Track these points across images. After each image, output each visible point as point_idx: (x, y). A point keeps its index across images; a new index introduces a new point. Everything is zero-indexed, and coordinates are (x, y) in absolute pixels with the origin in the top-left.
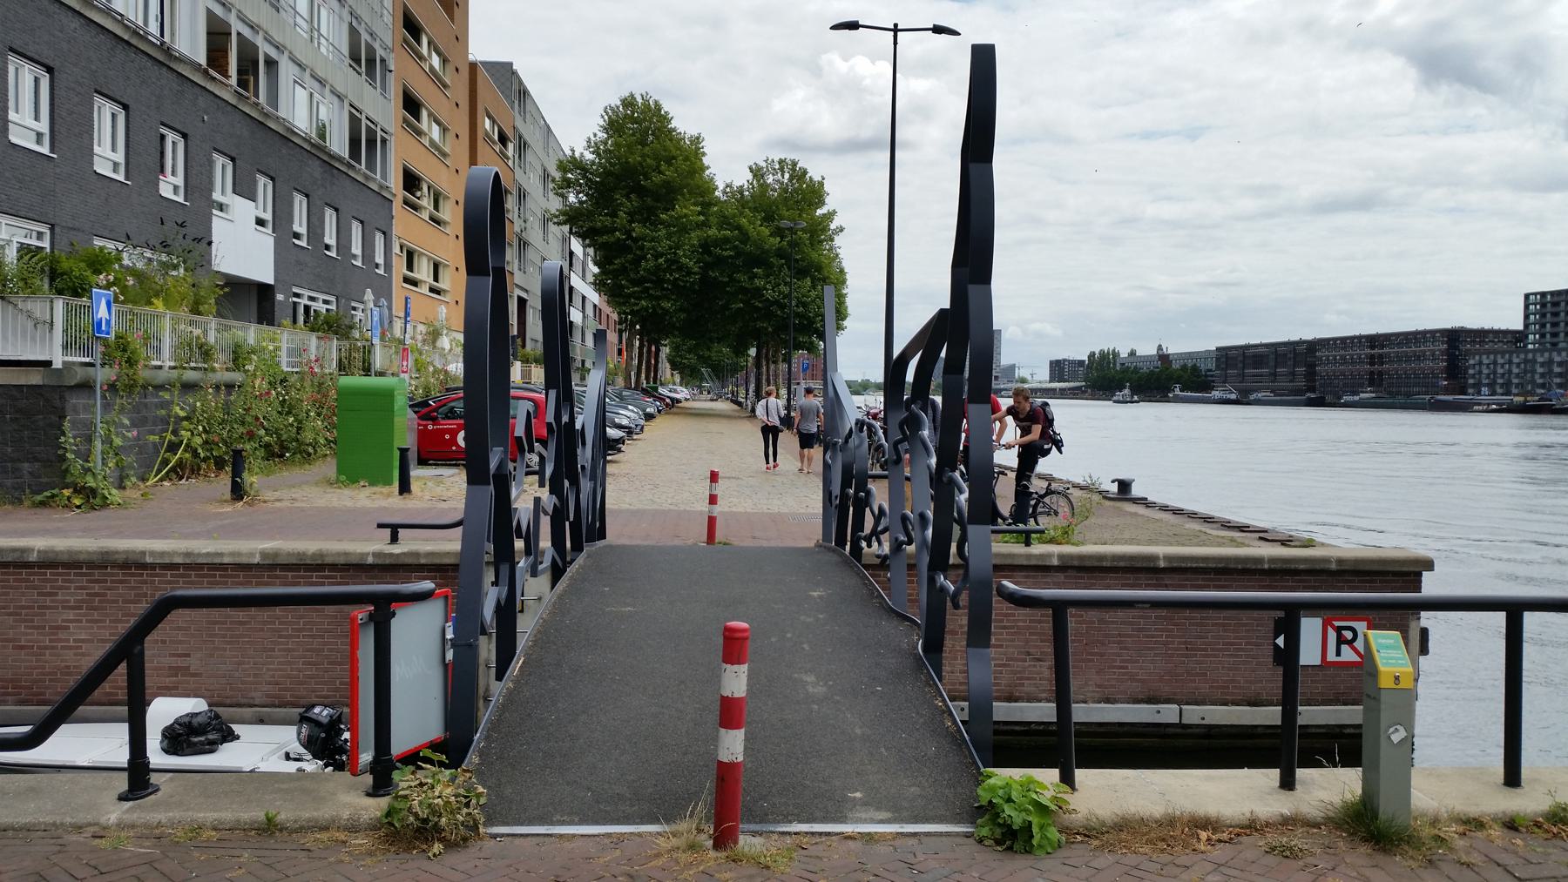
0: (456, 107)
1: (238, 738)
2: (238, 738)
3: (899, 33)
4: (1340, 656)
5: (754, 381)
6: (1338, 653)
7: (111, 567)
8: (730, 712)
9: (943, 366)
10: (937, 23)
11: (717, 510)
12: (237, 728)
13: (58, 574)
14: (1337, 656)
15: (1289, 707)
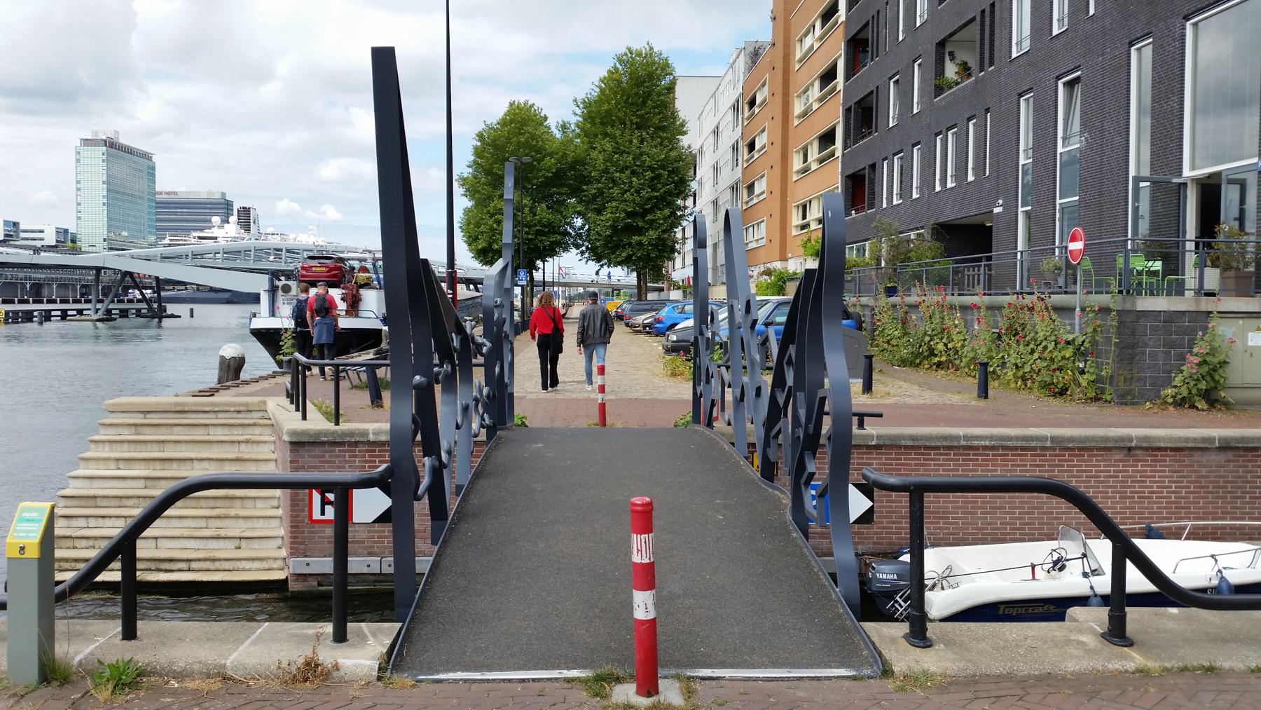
0: (1253, 355)
1: (976, 582)
2: (976, 582)
3: (1081, 560)
4: (324, 515)
5: (941, 401)
6: (323, 513)
7: (904, 447)
8: (647, 577)
9: (723, 250)
10: (1060, 623)
11: (608, 396)
12: (976, 579)
13: (881, 454)
14: (322, 515)
15: (341, 553)
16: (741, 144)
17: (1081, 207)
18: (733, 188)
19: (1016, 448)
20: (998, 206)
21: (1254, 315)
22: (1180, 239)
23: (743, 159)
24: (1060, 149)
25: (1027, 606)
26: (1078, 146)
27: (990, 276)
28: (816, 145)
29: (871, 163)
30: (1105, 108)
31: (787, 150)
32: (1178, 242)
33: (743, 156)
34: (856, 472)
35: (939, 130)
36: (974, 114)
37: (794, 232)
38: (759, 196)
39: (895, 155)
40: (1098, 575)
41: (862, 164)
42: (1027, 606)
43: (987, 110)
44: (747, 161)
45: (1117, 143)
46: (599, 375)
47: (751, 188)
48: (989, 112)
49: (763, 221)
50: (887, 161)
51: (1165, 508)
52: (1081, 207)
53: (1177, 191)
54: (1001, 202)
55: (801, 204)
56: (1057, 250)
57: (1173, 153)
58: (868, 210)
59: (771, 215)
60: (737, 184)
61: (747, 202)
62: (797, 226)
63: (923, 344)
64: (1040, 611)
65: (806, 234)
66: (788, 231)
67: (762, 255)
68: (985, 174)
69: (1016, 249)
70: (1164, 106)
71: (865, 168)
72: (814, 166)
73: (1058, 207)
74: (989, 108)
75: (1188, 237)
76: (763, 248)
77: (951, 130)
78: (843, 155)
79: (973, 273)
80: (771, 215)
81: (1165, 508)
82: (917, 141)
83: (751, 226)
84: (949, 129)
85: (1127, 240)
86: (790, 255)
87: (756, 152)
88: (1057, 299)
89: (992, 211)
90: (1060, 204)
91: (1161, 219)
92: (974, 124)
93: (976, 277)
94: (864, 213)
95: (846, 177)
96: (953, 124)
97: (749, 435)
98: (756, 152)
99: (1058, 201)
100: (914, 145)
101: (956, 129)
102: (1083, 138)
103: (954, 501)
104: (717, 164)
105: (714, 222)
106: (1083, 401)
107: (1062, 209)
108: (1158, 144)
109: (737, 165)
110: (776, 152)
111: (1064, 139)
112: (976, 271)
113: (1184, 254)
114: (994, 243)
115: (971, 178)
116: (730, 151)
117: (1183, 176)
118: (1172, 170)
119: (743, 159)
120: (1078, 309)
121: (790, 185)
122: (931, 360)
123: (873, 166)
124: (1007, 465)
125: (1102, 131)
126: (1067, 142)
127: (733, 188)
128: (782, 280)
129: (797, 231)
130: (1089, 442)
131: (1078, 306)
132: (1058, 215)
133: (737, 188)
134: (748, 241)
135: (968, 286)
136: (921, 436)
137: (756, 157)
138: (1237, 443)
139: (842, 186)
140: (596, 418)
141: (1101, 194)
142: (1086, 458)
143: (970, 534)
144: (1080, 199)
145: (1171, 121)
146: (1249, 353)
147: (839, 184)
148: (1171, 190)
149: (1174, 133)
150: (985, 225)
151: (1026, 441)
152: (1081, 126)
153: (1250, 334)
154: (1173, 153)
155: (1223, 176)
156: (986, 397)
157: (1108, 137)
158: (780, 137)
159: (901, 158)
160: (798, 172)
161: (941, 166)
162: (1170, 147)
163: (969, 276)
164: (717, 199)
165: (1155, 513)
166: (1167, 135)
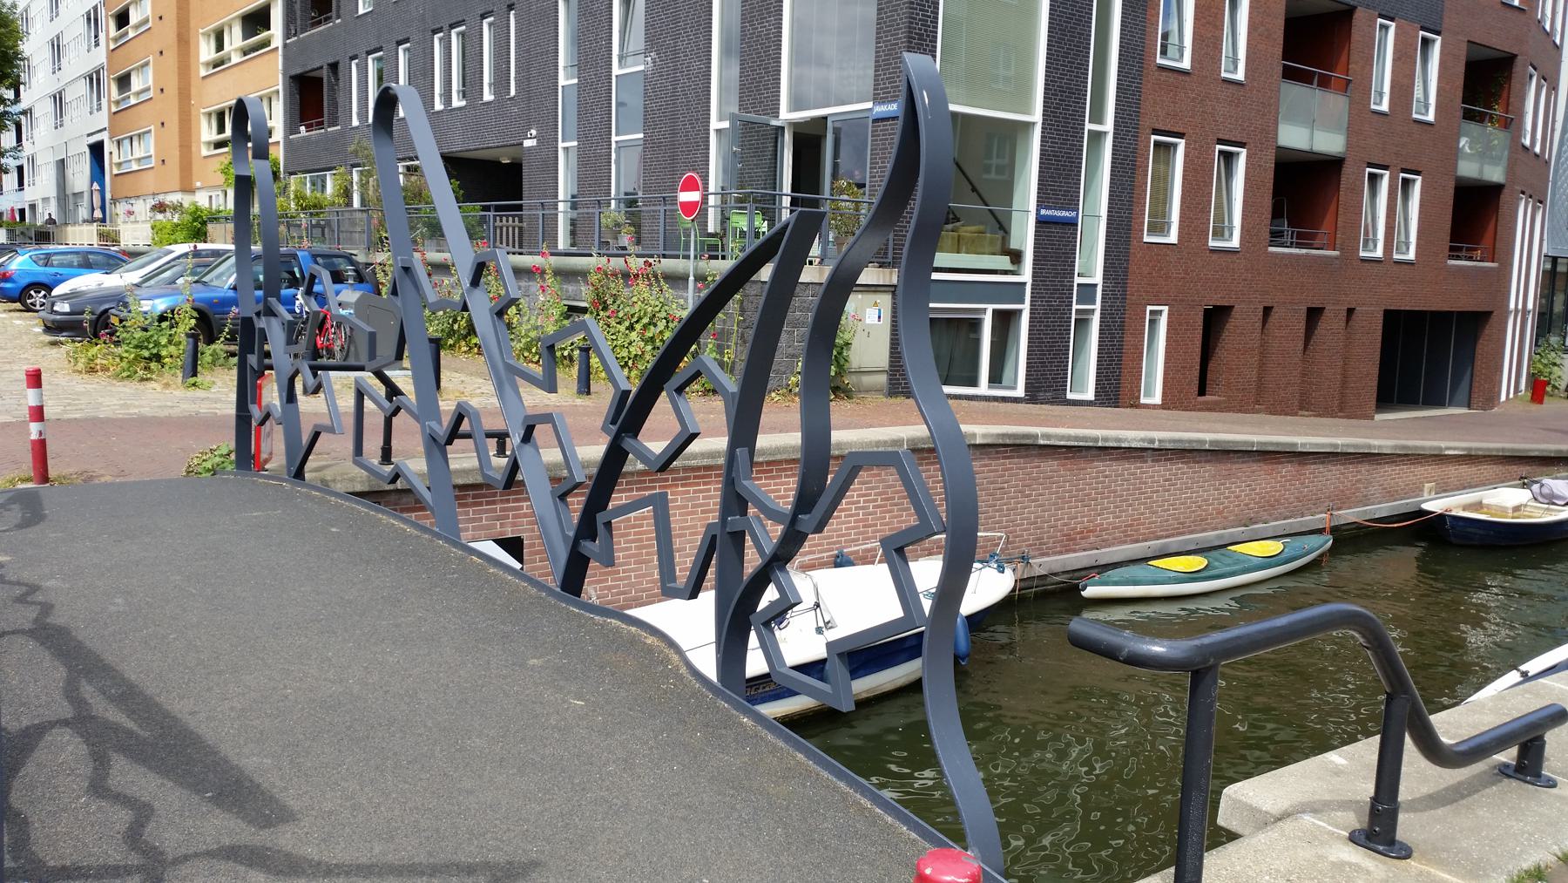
16: (102, 13)
17: (647, 148)
18: (91, 80)
19: (698, 468)
20: (531, 138)
21: (879, 289)
22: (777, 192)
23: (107, 35)
24: (616, 70)
25: (755, 685)
26: (641, 68)
27: (521, 229)
28: (237, 30)
29: (331, 60)
30: (679, 22)
31: (188, 31)
32: (775, 195)
33: (107, 32)
34: (498, 523)
35: (439, 26)
36: (490, 9)
37: (205, 152)
38: (138, 94)
39: (369, 53)
40: (831, 628)
41: (316, 61)
42: (755, 685)
43: (511, 7)
44: (116, 40)
45: (694, 70)
46: (28, 387)
47: (124, 82)
48: (512, 9)
49: (149, 131)
50: (357, 61)
51: (853, 528)
52: (647, 148)
53: (774, 136)
54: (534, 132)
55: (215, 111)
56: (613, 202)
57: (769, 89)
58: (329, 127)
59: (163, 124)
60: (98, 72)
61: (117, 103)
62: (209, 143)
63: (459, 318)
64: (772, 688)
65: (226, 155)
66: (194, 149)
67: (149, 182)
68: (509, 93)
69: (556, 196)
70: (757, 28)
71: (321, 67)
72: (236, 58)
73: (614, 146)
74: (513, 5)
75: (785, 191)
76: (150, 172)
77: (454, 28)
78: (285, 46)
79: (500, 224)
80: (163, 124)
81: (853, 528)
82: (405, 37)
83: (126, 138)
84: (452, 26)
85: (610, 200)
86: (198, 184)
87: (132, 27)
88: (668, 264)
89: (522, 144)
90: (616, 142)
91: (753, 169)
92: (490, 25)
93: (505, 229)
94: (323, 131)
95: (291, 77)
96: (460, 19)
97: (334, 481)
98: (132, 27)
99: (614, 138)
100: (399, 43)
101: (464, 28)
102: (649, 59)
103: (627, 547)
104: (58, 38)
105: (56, 128)
106: (700, 393)
107: (619, 148)
108: (749, 75)
109: (97, 45)
110: (167, 34)
111: (621, 58)
112: (517, 223)
113: (780, 210)
114: (525, 186)
115: (488, 96)
116: (82, 22)
117: (780, 118)
118: (767, 110)
119: (107, 35)
120: (691, 278)
121: (195, 83)
122: (470, 340)
123: (334, 67)
124: (688, 492)
125: (675, 52)
126: (623, 61)
127: (91, 80)
128: (200, 220)
129: (209, 150)
130: (781, 454)
131: (691, 274)
132: (613, 156)
133: (98, 80)
134: (122, 160)
135: (501, 243)
136: (587, 462)
137: (131, 34)
138: (924, 443)
139: (284, 89)
140: (27, 465)
141: (674, 133)
142: (774, 473)
143: (644, 590)
144: (579, 145)
145: (766, 47)
146: (867, 331)
147: (280, 87)
148: (766, 135)
149: (770, 63)
150: (500, 163)
151: (713, 458)
152: (646, 42)
153: (868, 310)
154: (769, 89)
155: (830, 124)
156: (588, 393)
157: (683, 60)
158: (175, 11)
159: (379, 59)
160: (207, 64)
161: (358, 86)
162: (765, 81)
163: (507, 228)
164: (60, 93)
165: (843, 535)
166: (761, 65)
